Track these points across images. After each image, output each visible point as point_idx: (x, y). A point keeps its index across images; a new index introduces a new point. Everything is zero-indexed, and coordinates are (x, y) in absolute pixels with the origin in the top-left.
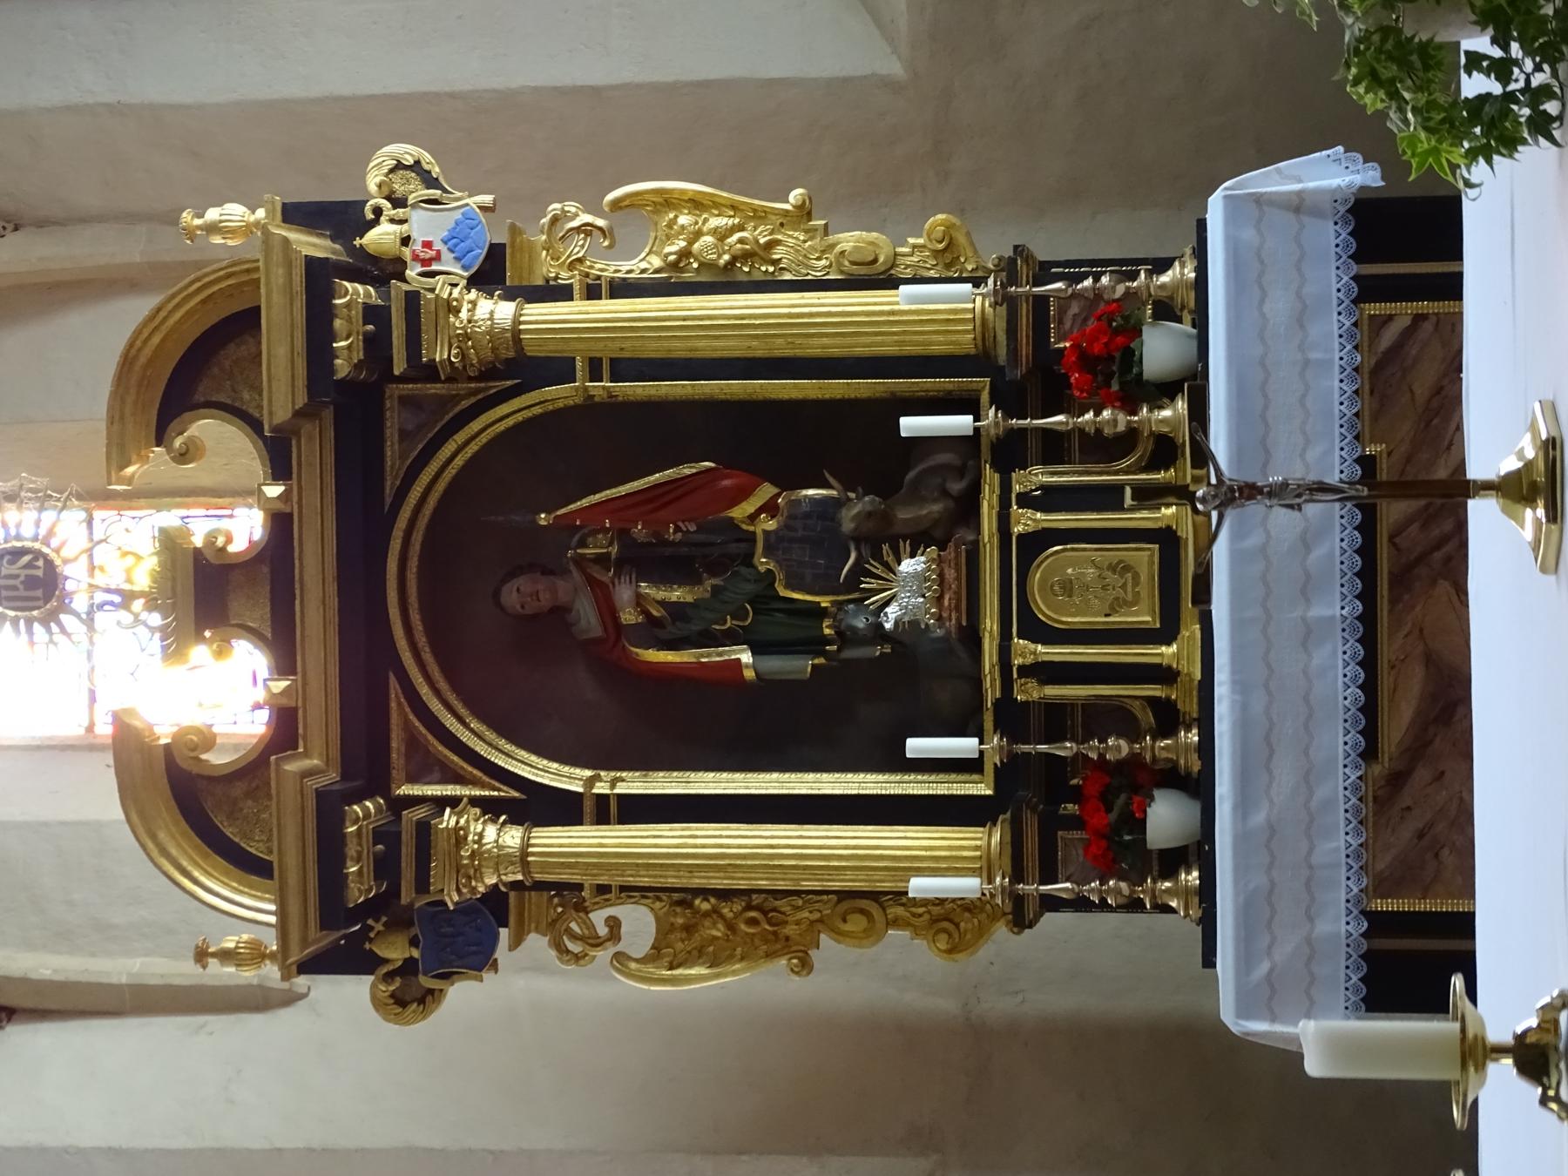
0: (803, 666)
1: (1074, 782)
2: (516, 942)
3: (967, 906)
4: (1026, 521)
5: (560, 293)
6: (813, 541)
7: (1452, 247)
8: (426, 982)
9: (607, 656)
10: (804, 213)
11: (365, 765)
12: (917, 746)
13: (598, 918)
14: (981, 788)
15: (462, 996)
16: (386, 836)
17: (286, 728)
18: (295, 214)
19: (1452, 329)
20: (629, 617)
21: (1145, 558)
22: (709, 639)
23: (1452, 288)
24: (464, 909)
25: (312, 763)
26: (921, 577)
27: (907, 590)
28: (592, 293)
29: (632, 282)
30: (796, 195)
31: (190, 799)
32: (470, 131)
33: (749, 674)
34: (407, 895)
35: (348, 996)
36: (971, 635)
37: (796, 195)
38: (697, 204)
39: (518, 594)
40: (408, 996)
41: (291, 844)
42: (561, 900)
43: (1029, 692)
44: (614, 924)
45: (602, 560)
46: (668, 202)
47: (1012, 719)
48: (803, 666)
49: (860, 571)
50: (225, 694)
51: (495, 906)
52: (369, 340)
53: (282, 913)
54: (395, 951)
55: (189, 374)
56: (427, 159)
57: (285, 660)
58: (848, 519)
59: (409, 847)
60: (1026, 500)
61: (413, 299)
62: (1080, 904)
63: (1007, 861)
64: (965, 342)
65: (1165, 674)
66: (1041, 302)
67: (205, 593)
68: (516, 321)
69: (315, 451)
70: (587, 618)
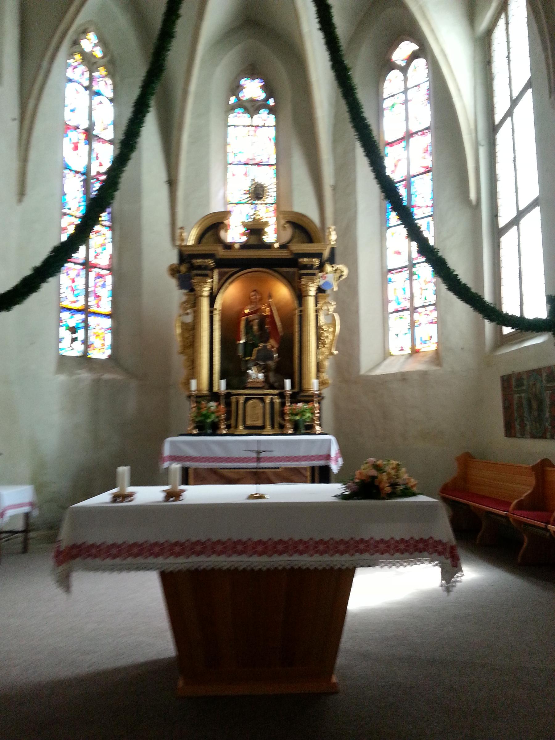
0: (241, 353)
2: (186, 294)
4: (268, 399)
5: (317, 302)
6: (266, 356)
7: (321, 482)
10: (332, 354)
11: (221, 263)
15: (173, 283)
16: (206, 268)
17: (229, 247)
18: (333, 250)
19: (305, 482)
21: (259, 423)
22: (247, 333)
23: (313, 482)
24: (191, 284)
25: (221, 253)
26: (257, 378)
27: (256, 375)
28: (317, 311)
30: (336, 352)
31: (215, 226)
32: (350, 286)
33: (238, 342)
34: (195, 272)
35: (174, 259)
36: (245, 388)
37: (336, 352)
38: (334, 332)
40: (174, 271)
41: (204, 248)
42: (193, 303)
43: (234, 399)
44: (187, 314)
46: (334, 326)
48: (241, 353)
49: (260, 365)
50: (235, 234)
51: (192, 290)
52: (306, 266)
53: (189, 246)
54: (183, 269)
55: (300, 228)
56: (344, 277)
57: (244, 246)
58: (270, 363)
60: (272, 399)
61: (314, 274)
63: (199, 395)
64: (305, 387)
65: (236, 427)
67: (255, 230)
68: (310, 296)
69: (284, 254)
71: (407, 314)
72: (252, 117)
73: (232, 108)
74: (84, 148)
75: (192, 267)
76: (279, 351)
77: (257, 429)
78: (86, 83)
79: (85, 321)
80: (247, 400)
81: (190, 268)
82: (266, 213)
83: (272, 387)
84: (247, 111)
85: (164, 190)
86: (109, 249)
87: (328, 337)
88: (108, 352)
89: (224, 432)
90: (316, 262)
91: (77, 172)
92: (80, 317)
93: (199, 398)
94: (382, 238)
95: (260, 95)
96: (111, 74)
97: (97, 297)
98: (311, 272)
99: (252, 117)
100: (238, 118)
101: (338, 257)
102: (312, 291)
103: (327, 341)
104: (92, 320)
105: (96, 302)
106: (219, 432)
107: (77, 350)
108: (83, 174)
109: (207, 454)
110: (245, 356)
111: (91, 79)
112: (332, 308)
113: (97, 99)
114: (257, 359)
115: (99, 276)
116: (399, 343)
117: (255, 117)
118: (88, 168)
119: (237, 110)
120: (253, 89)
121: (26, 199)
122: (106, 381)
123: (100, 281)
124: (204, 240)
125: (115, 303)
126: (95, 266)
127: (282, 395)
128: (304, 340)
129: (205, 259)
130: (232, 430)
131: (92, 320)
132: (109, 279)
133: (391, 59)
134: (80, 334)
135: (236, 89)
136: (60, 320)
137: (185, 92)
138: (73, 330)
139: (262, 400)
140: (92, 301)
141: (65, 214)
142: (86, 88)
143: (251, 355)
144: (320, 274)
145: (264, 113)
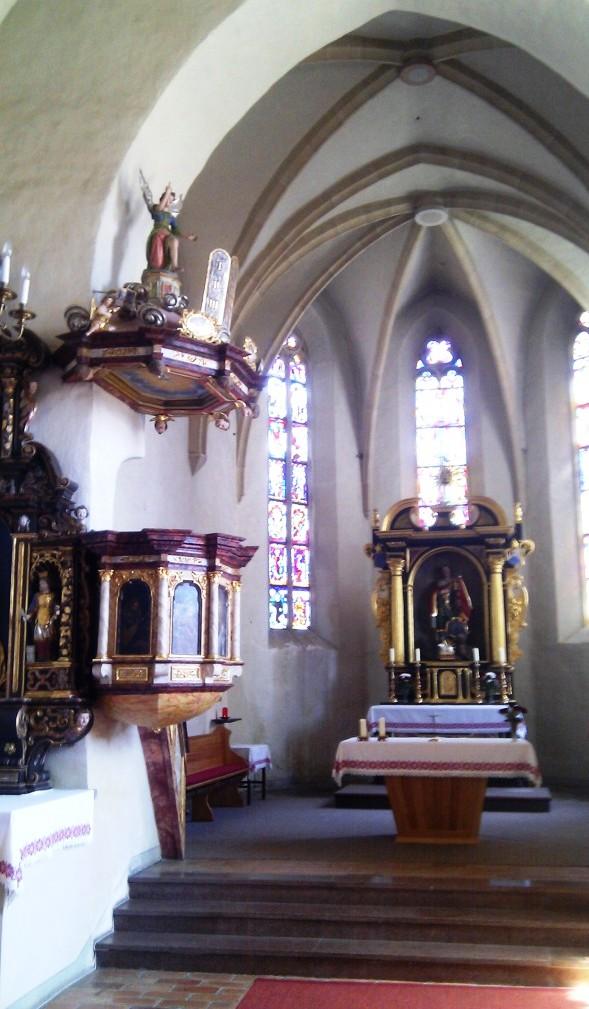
0: (434, 625)
1: (136, 604)
2: (380, 572)
3: (389, 658)
4: (459, 671)
5: (504, 579)
8: (372, 555)
9: (435, 587)
11: (412, 543)
12: (418, 651)
13: (385, 587)
14: (411, 660)
15: (369, 562)
20: (443, 592)
21: (453, 693)
22: (438, 607)
25: (409, 533)
26: (447, 651)
27: (447, 648)
29: (506, 597)
30: (525, 624)
31: (404, 512)
34: (388, 553)
35: (368, 540)
39: (447, 570)
45: (453, 587)
47: (423, 667)
50: (427, 518)
51: (386, 567)
54: (378, 548)
57: (432, 529)
58: (461, 636)
59: (398, 553)
62: (390, 680)
64: (495, 659)
65: (432, 696)
66: (388, 725)
67: (444, 513)
69: (471, 533)
70: (443, 583)
72: (439, 380)
73: (420, 373)
74: (284, 436)
75: (386, 548)
76: (469, 623)
77: (449, 699)
78: (283, 375)
79: (289, 597)
80: (439, 673)
81: (382, 550)
82: (456, 494)
84: (433, 373)
85: (356, 463)
86: (307, 526)
88: (308, 624)
89: (421, 701)
90: (503, 541)
91: (277, 459)
92: (284, 592)
93: (399, 670)
95: (447, 357)
96: (304, 361)
97: (298, 571)
99: (439, 380)
100: (426, 383)
101: (524, 532)
102: (499, 568)
103: (517, 613)
104: (296, 594)
105: (296, 577)
106: (416, 701)
107: (283, 623)
108: (282, 460)
109: (408, 721)
110: (438, 627)
111: (288, 368)
112: (519, 582)
113: (294, 385)
114: (450, 631)
115: (300, 552)
117: (444, 379)
118: (288, 454)
119: (425, 374)
120: (439, 351)
121: (244, 498)
122: (310, 652)
123: (300, 557)
124: (397, 525)
125: (312, 577)
126: (295, 543)
127: (472, 667)
128: (493, 615)
130: (428, 700)
131: (296, 594)
132: (307, 554)
133: (579, 321)
134: (285, 607)
135: (422, 353)
136: (270, 597)
137: (375, 376)
138: (278, 605)
139: (455, 672)
140: (294, 577)
141: (271, 499)
142: (283, 380)
143: (444, 628)
144: (508, 550)
145: (451, 374)
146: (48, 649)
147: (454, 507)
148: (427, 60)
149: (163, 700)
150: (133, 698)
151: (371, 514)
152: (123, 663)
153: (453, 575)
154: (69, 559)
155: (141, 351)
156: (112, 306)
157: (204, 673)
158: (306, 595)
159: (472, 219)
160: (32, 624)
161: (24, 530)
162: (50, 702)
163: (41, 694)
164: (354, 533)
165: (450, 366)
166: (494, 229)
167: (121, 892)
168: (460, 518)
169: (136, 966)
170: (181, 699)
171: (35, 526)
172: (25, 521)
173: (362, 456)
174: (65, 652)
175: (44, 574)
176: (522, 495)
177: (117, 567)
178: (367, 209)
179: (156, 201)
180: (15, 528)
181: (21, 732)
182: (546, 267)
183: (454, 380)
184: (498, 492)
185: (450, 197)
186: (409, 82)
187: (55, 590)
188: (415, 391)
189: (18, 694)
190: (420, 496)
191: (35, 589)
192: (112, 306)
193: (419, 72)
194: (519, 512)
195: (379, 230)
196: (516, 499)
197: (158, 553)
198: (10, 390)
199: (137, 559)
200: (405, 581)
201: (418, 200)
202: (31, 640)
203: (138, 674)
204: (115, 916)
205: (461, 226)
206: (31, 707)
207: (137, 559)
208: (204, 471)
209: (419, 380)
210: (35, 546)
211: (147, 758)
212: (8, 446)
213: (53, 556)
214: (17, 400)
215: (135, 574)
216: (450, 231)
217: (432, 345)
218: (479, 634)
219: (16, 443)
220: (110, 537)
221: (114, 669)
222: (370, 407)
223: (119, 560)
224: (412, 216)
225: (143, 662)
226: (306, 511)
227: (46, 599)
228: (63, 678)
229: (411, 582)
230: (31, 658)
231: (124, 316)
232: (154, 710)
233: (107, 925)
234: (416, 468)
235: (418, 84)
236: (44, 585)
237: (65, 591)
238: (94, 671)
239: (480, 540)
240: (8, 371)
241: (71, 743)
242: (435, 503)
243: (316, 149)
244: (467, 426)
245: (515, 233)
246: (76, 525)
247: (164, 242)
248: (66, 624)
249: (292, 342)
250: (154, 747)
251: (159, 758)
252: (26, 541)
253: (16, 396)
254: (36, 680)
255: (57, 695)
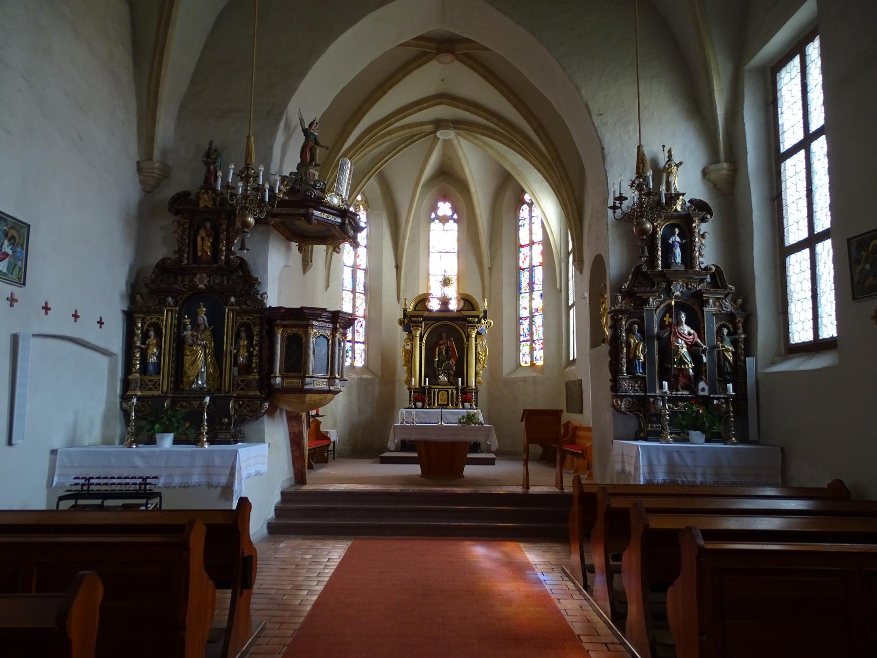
4: (450, 391)
5: (476, 341)
6: (449, 368)
9: (437, 344)
11: (426, 319)
15: (400, 328)
18: (485, 312)
21: (446, 403)
25: (426, 314)
27: (443, 378)
29: (477, 348)
31: (423, 300)
35: (400, 315)
39: (444, 335)
40: (401, 322)
42: (411, 339)
47: (430, 388)
50: (434, 305)
51: (410, 332)
54: (406, 321)
59: (418, 324)
67: (445, 302)
69: (459, 315)
70: (442, 342)
71: (528, 343)
73: (433, 220)
75: (410, 321)
81: (409, 322)
82: (452, 292)
83: (452, 385)
84: (441, 221)
87: (482, 357)
94: (517, 300)
95: (449, 213)
96: (366, 209)
98: (473, 325)
100: (436, 226)
116: (525, 360)
120: (445, 208)
127: (457, 389)
129: (416, 317)
132: (364, 323)
135: (435, 208)
137: (407, 220)
145: (451, 222)
146: (246, 369)
147: (451, 299)
148: (452, 52)
149: (309, 397)
150: (292, 396)
151: (402, 300)
152: (288, 377)
153: (448, 338)
154: (257, 321)
155: (302, 211)
156: (287, 185)
157: (330, 384)
158: (362, 346)
159: (469, 137)
160: (236, 356)
161: (232, 304)
162: (247, 397)
163: (241, 393)
164: (393, 312)
165: (451, 218)
166: (481, 144)
167: (278, 498)
168: (453, 306)
169: (290, 533)
170: (317, 397)
171: (238, 303)
172: (233, 299)
173: (398, 267)
174: (255, 371)
175: (243, 329)
176: (487, 294)
177: (284, 326)
178: (410, 126)
179: (307, 127)
180: (227, 303)
181: (232, 412)
182: (508, 168)
183: (452, 226)
184: (476, 295)
185: (456, 124)
186: (440, 62)
187: (250, 338)
188: (429, 230)
189: (229, 392)
190: (430, 292)
191: (238, 337)
192: (287, 185)
193: (447, 57)
194: (486, 304)
195: (415, 138)
196: (484, 297)
197: (308, 320)
198: (225, 227)
199: (295, 322)
200: (421, 340)
201: (439, 124)
202: (236, 364)
203: (296, 382)
204: (276, 509)
205: (463, 142)
206: (236, 400)
207: (295, 322)
208: (309, 273)
209: (432, 225)
210: (238, 313)
211: (290, 430)
212: (223, 258)
213: (248, 319)
214: (228, 232)
215: (295, 330)
216: (455, 142)
217: (440, 204)
218: (461, 370)
219: (227, 256)
220: (283, 310)
221: (282, 380)
222: (404, 239)
223: (285, 322)
224: (435, 132)
225: (299, 377)
226: (364, 297)
227: (244, 342)
228: (254, 384)
229: (424, 341)
230: (236, 373)
231: (292, 191)
232: (304, 402)
233: (272, 514)
234: (428, 275)
235: (445, 63)
236: (243, 334)
237: (255, 338)
238: (272, 381)
239: (464, 319)
240: (223, 216)
241: (257, 419)
242: (439, 296)
243: (385, 93)
244: (458, 253)
245: (491, 147)
246: (262, 303)
247: (311, 150)
248: (256, 356)
249: (359, 198)
250: (294, 424)
251: (297, 430)
252: (233, 310)
253: (227, 230)
254: (239, 385)
255: (251, 393)
